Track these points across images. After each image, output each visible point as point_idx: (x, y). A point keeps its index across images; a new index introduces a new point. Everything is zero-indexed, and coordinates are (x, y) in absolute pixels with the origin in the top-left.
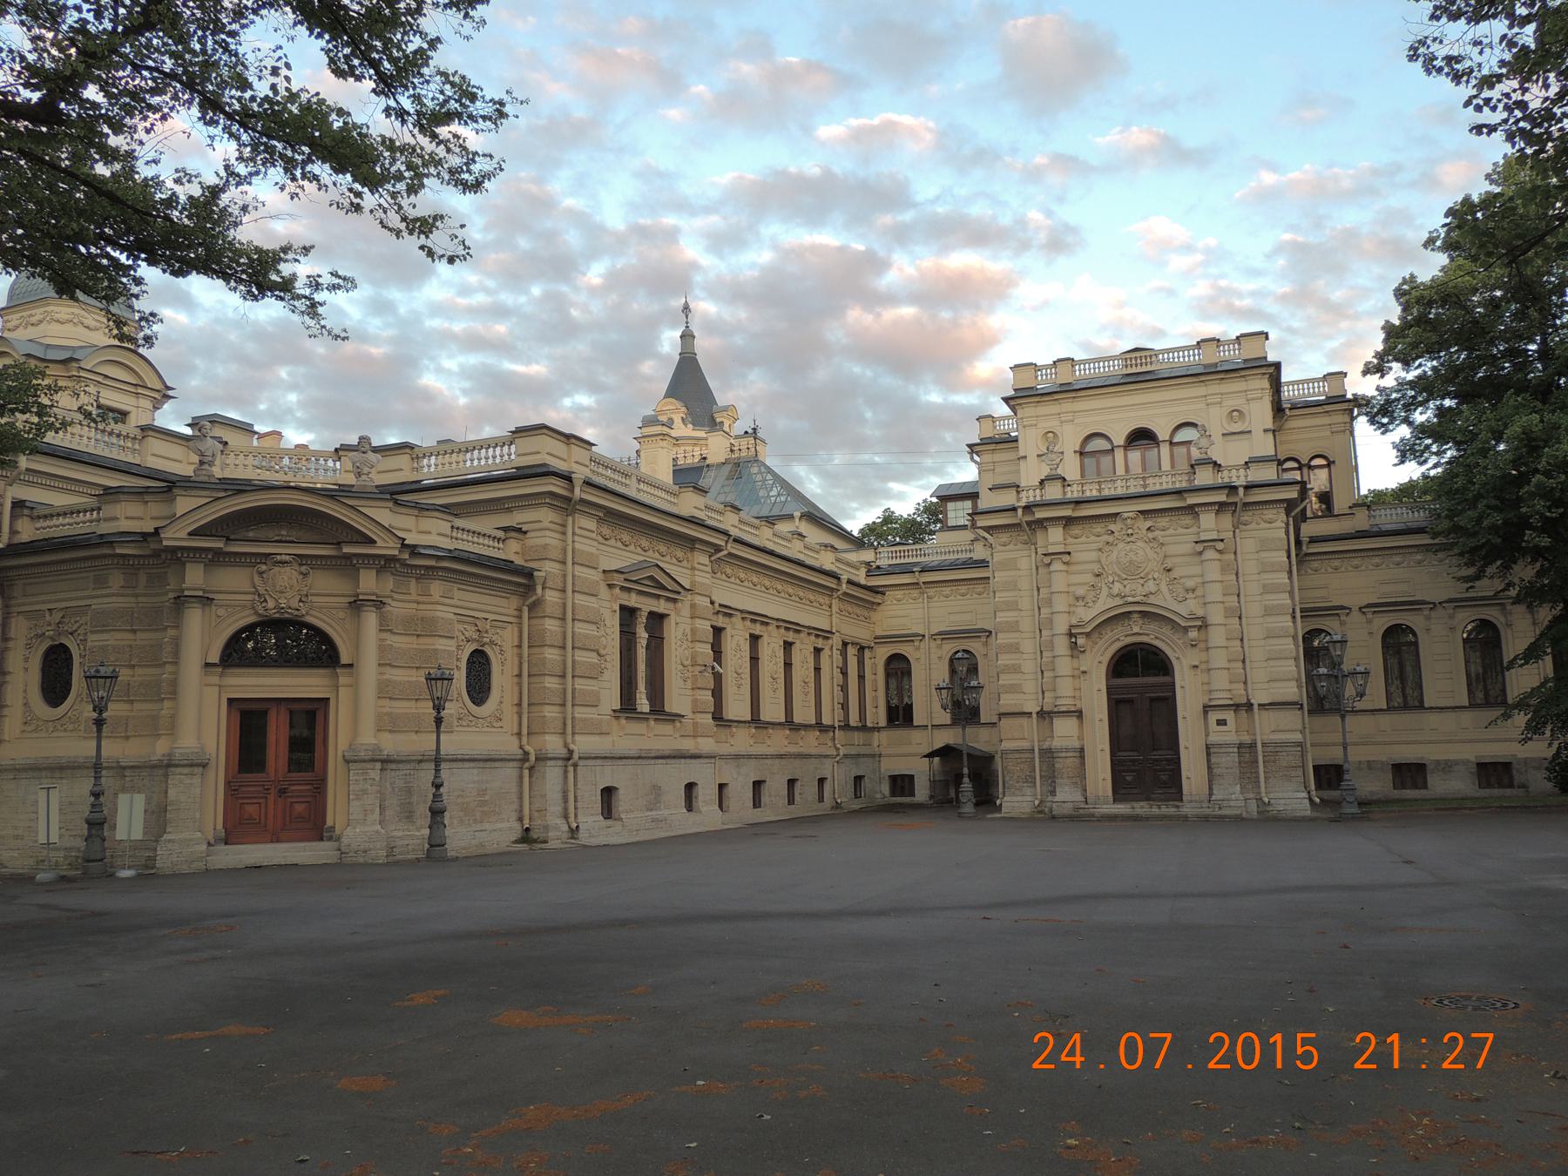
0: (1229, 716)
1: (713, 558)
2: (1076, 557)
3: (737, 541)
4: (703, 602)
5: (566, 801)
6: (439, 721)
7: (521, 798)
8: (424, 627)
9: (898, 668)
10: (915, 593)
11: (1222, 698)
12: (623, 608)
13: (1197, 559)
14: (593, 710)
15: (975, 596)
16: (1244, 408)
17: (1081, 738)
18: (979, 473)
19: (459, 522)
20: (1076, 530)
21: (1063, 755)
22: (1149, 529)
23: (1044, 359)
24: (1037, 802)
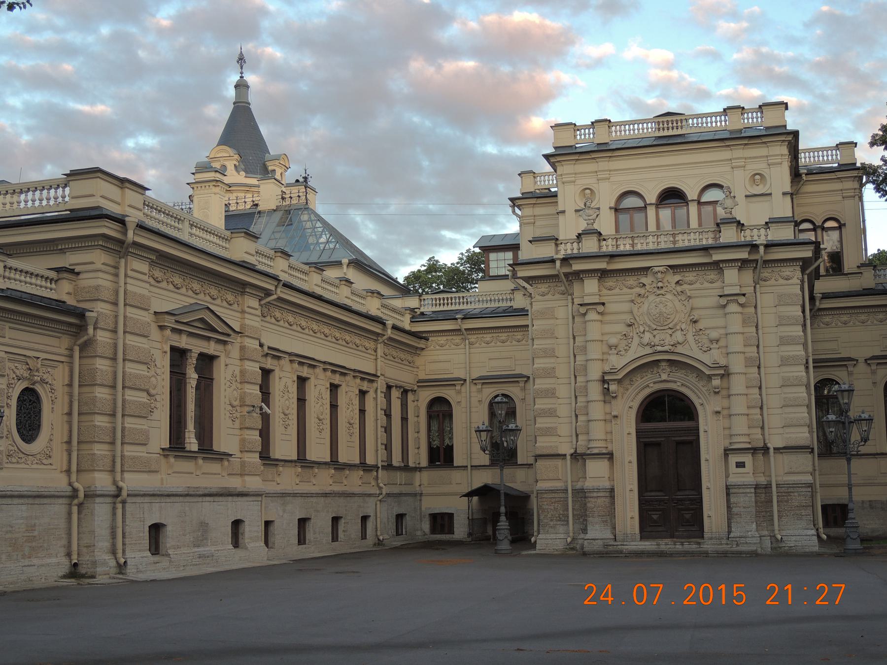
0: (747, 459)
1: (263, 302)
2: (610, 307)
3: (287, 286)
4: (253, 344)
10: (457, 339)
11: (741, 442)
17: (611, 479)
20: (610, 282)
21: (595, 494)
22: (677, 283)
23: (583, 120)
24: (569, 540)
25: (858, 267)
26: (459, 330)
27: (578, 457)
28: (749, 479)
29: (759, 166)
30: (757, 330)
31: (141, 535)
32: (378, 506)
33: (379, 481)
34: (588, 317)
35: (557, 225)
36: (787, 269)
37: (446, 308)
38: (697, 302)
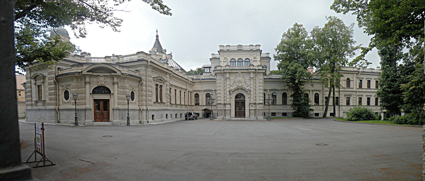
0: (253, 105)
2: (231, 79)
3: (174, 73)
5: (147, 117)
6: (128, 103)
7: (139, 116)
8: (124, 88)
9: (197, 96)
10: (200, 83)
11: (252, 102)
12: (156, 84)
13: (249, 80)
14: (151, 102)
19: (129, 69)
20: (231, 74)
26: (200, 82)
27: (225, 104)
28: (253, 108)
29: (255, 56)
37: (198, 78)
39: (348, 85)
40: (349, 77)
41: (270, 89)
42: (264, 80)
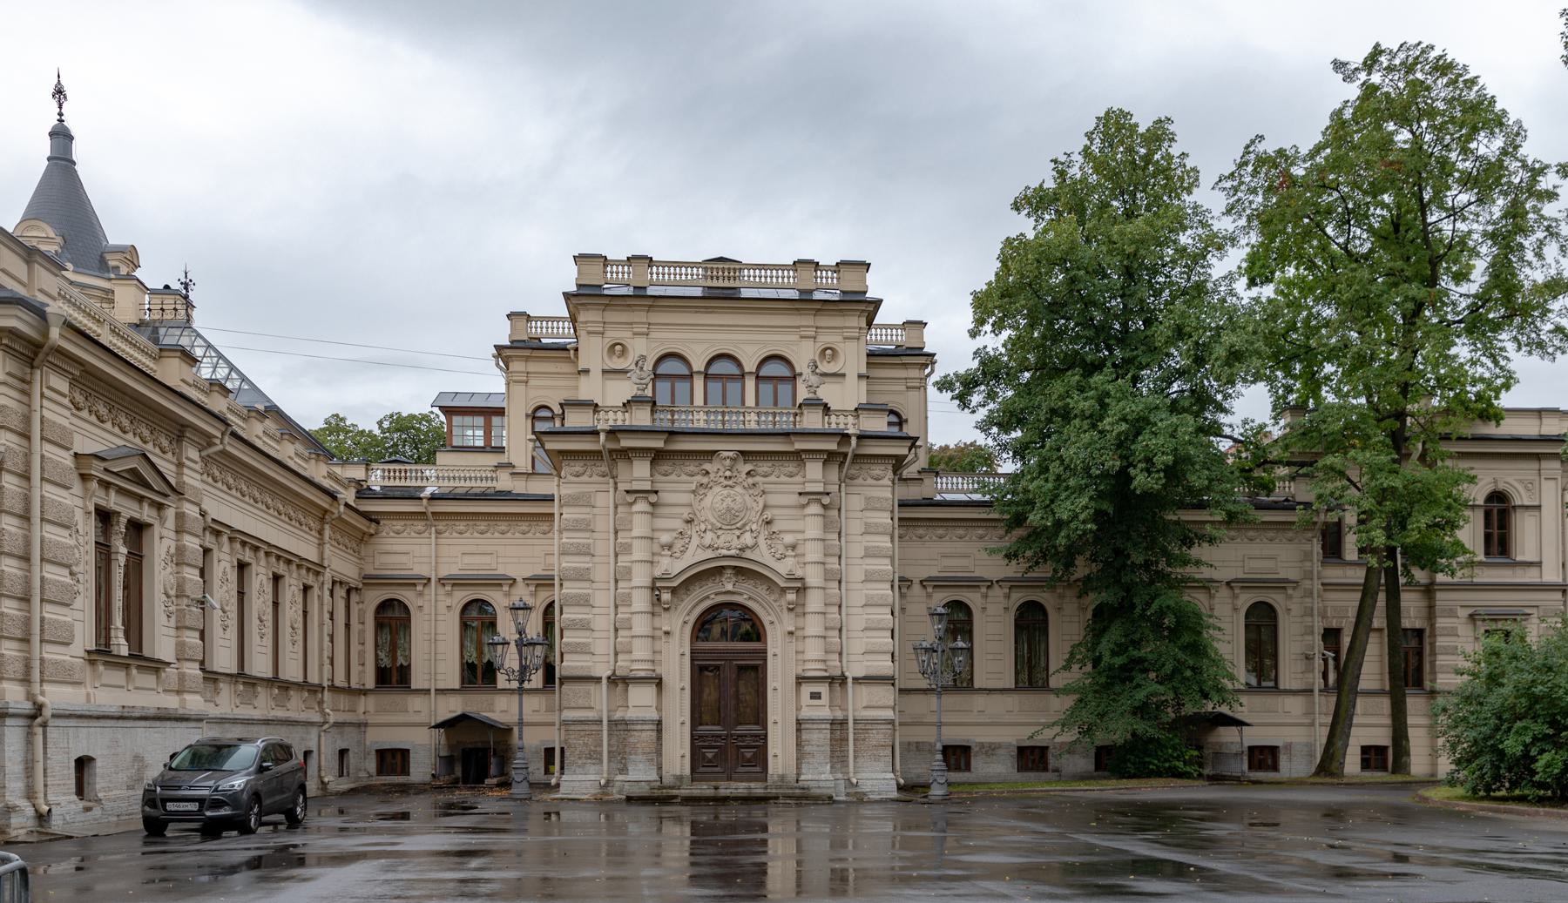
0: (823, 689)
1: (204, 453)
2: (666, 497)
3: (234, 435)
4: (191, 511)
10: (420, 525)
11: (814, 669)
15: (497, 535)
16: (840, 347)
18: (508, 384)
21: (639, 727)
22: (748, 473)
23: (617, 253)
24: (603, 782)
25: (919, 472)
27: (619, 681)
30: (840, 538)
31: (65, 772)
32: (323, 739)
33: (325, 705)
34: (636, 508)
35: (868, 392)
36: (878, 467)
38: (773, 499)
39: (1499, 541)
40: (1501, 486)
41: (925, 576)
42: (896, 517)
